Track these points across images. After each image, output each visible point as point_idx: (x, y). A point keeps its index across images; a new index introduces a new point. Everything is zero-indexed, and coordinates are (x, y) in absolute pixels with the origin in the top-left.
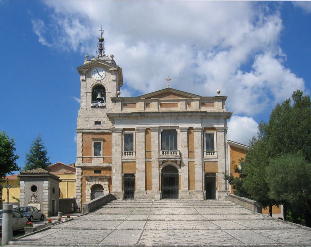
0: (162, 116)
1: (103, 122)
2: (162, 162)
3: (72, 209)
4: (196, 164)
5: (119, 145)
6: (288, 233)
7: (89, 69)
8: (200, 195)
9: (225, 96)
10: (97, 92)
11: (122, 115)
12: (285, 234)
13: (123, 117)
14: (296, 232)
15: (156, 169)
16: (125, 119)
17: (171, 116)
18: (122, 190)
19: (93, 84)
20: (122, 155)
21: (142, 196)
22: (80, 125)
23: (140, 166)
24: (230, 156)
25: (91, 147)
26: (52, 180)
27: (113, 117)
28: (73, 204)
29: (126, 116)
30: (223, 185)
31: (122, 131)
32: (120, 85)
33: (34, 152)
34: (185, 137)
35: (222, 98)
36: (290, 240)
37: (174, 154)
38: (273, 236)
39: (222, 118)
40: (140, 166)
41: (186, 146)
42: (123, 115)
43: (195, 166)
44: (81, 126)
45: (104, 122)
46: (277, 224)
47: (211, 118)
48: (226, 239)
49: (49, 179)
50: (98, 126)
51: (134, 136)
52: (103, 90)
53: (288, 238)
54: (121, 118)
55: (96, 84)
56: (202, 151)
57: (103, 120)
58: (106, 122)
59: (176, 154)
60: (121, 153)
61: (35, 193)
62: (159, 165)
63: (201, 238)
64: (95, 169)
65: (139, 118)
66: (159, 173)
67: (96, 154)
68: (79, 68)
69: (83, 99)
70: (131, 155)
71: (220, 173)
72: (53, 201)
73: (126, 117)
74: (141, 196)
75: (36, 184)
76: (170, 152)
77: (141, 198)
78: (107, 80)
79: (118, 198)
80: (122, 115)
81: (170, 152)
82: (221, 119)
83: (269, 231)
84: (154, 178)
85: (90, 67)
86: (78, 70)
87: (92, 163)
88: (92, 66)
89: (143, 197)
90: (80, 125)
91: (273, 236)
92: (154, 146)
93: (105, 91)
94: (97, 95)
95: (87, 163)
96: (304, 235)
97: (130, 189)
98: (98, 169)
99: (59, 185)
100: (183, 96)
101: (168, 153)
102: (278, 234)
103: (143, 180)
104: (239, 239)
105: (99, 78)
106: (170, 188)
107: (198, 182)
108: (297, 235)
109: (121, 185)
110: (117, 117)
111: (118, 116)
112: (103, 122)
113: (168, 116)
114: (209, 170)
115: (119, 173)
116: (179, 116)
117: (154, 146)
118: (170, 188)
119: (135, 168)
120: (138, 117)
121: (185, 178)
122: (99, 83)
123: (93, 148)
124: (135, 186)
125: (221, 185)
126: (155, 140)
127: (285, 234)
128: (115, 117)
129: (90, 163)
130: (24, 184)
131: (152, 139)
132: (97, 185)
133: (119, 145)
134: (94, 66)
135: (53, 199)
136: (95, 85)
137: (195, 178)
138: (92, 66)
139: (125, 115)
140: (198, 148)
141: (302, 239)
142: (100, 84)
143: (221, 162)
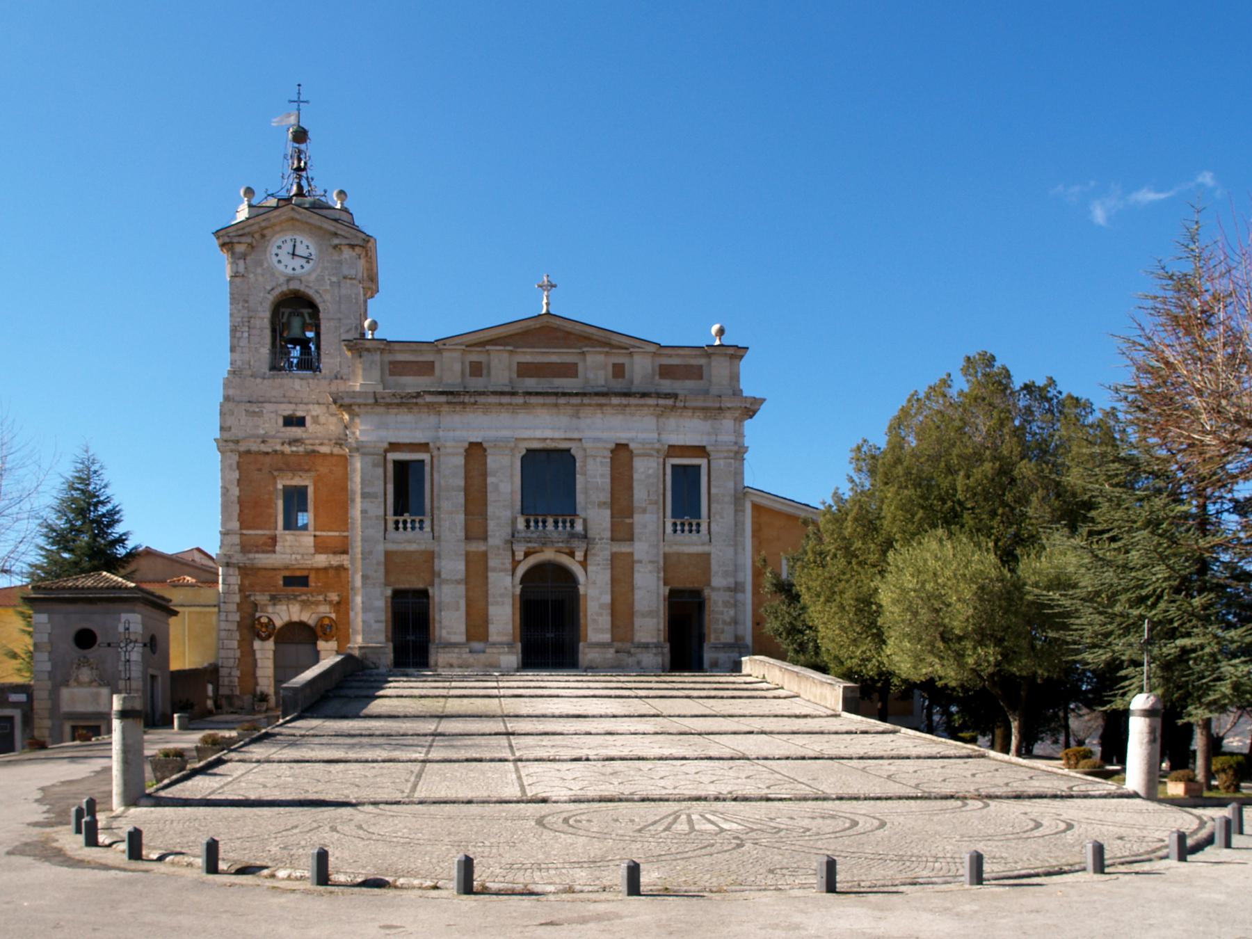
0: (526, 405)
1: (313, 417)
2: (522, 554)
3: (210, 703)
4: (640, 562)
5: (374, 496)
6: (943, 767)
7: (257, 236)
8: (651, 656)
9: (740, 345)
10: (290, 315)
11: (383, 398)
12: (937, 771)
13: (388, 405)
14: (966, 766)
15: (502, 574)
16: (395, 411)
17: (556, 405)
18: (387, 640)
19: (273, 289)
20: (386, 530)
21: (455, 661)
22: (230, 428)
23: (452, 566)
24: (753, 536)
25: (271, 504)
26: (150, 611)
27: (351, 405)
28: (210, 688)
29: (399, 401)
30: (726, 628)
31: (386, 451)
32: (369, 293)
33: (71, 516)
34: (602, 476)
35: (731, 351)
36: (950, 785)
37: (564, 527)
38: (903, 776)
39: (728, 414)
40: (452, 566)
41: (605, 503)
42: (388, 400)
43: (637, 567)
44: (233, 430)
45: (316, 420)
46: (911, 745)
47: (690, 414)
48: (772, 782)
49: (140, 607)
50: (296, 432)
51: (427, 469)
52: (310, 311)
53: (944, 780)
54: (381, 410)
55: (285, 288)
56: (658, 518)
57: (314, 413)
58: (322, 419)
59: (572, 525)
60: (383, 522)
61: (91, 653)
62: (515, 564)
63: (450, 822)
64: (287, 573)
65: (445, 408)
66: (514, 586)
67: (290, 524)
68: (221, 233)
69: (239, 338)
70: (417, 530)
71: (719, 589)
72: (153, 677)
73: (399, 405)
74: (451, 661)
75: (93, 620)
76: (550, 521)
77: (451, 666)
78: (326, 278)
79: (373, 666)
80: (383, 398)
81: (550, 521)
82: (724, 418)
83: (890, 764)
84: (497, 603)
85: (263, 229)
86: (218, 238)
87: (274, 552)
88: (266, 228)
89: (460, 661)
90: (230, 428)
91: (903, 776)
92: (496, 501)
93: (318, 316)
94: (287, 325)
95: (257, 552)
96: (989, 774)
97: (408, 638)
98: (298, 573)
99: (168, 624)
100: (597, 340)
101: (544, 522)
102: (915, 772)
103: (457, 610)
104: (809, 782)
105: (294, 269)
106: (550, 635)
107: (643, 616)
108: (968, 774)
109: (382, 626)
110: (365, 405)
111: (371, 401)
112: (313, 417)
113: (544, 405)
114: (685, 582)
115: (374, 584)
116: (582, 405)
117: (496, 501)
118: (550, 635)
119: (434, 574)
120: (441, 404)
121: (601, 606)
122: (294, 285)
123: (280, 504)
124: (431, 628)
125: (721, 626)
126: (501, 481)
127: (937, 771)
128: (359, 405)
129: (267, 552)
130: (49, 626)
131: (490, 480)
132: (295, 623)
133: (376, 497)
134: (278, 228)
135: (151, 671)
136: (283, 294)
137: (636, 604)
138: (266, 228)
139: (395, 401)
140: (644, 511)
141: (983, 783)
142: (299, 291)
143: (720, 554)
